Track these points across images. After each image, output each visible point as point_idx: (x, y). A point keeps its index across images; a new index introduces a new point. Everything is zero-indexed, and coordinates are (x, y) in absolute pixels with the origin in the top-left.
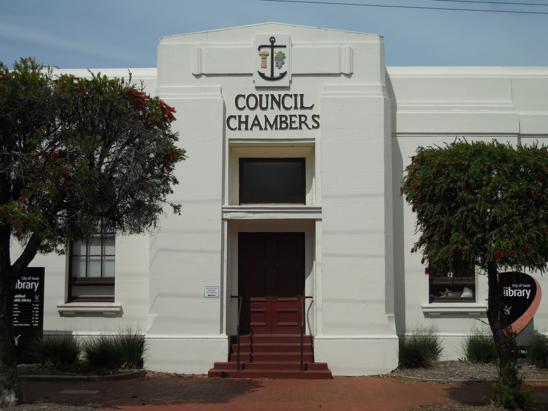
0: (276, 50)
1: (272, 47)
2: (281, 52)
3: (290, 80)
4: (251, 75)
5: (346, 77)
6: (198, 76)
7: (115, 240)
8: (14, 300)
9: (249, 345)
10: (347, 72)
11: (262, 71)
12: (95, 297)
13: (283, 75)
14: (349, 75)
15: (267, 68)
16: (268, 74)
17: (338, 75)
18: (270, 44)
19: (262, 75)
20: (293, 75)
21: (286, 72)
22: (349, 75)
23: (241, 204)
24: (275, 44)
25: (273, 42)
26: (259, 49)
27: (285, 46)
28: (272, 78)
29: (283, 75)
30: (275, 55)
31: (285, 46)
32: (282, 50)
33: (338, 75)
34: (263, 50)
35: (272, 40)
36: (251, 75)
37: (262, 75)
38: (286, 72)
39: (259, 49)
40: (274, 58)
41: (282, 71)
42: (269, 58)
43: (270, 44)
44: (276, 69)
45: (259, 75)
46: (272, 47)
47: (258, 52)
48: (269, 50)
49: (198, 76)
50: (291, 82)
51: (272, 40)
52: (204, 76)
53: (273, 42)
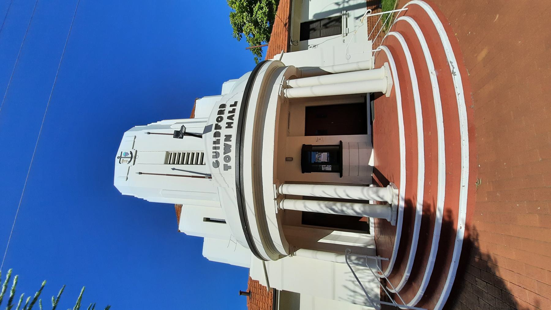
6: (127, 179)
10: (134, 138)
16: (129, 159)
17: (134, 141)
20: (133, 149)
26: (121, 163)
27: (122, 152)
30: (124, 157)
31: (122, 152)
32: (123, 153)
37: (130, 162)
39: (121, 163)
41: (129, 153)
42: (125, 159)
48: (122, 159)
49: (127, 179)
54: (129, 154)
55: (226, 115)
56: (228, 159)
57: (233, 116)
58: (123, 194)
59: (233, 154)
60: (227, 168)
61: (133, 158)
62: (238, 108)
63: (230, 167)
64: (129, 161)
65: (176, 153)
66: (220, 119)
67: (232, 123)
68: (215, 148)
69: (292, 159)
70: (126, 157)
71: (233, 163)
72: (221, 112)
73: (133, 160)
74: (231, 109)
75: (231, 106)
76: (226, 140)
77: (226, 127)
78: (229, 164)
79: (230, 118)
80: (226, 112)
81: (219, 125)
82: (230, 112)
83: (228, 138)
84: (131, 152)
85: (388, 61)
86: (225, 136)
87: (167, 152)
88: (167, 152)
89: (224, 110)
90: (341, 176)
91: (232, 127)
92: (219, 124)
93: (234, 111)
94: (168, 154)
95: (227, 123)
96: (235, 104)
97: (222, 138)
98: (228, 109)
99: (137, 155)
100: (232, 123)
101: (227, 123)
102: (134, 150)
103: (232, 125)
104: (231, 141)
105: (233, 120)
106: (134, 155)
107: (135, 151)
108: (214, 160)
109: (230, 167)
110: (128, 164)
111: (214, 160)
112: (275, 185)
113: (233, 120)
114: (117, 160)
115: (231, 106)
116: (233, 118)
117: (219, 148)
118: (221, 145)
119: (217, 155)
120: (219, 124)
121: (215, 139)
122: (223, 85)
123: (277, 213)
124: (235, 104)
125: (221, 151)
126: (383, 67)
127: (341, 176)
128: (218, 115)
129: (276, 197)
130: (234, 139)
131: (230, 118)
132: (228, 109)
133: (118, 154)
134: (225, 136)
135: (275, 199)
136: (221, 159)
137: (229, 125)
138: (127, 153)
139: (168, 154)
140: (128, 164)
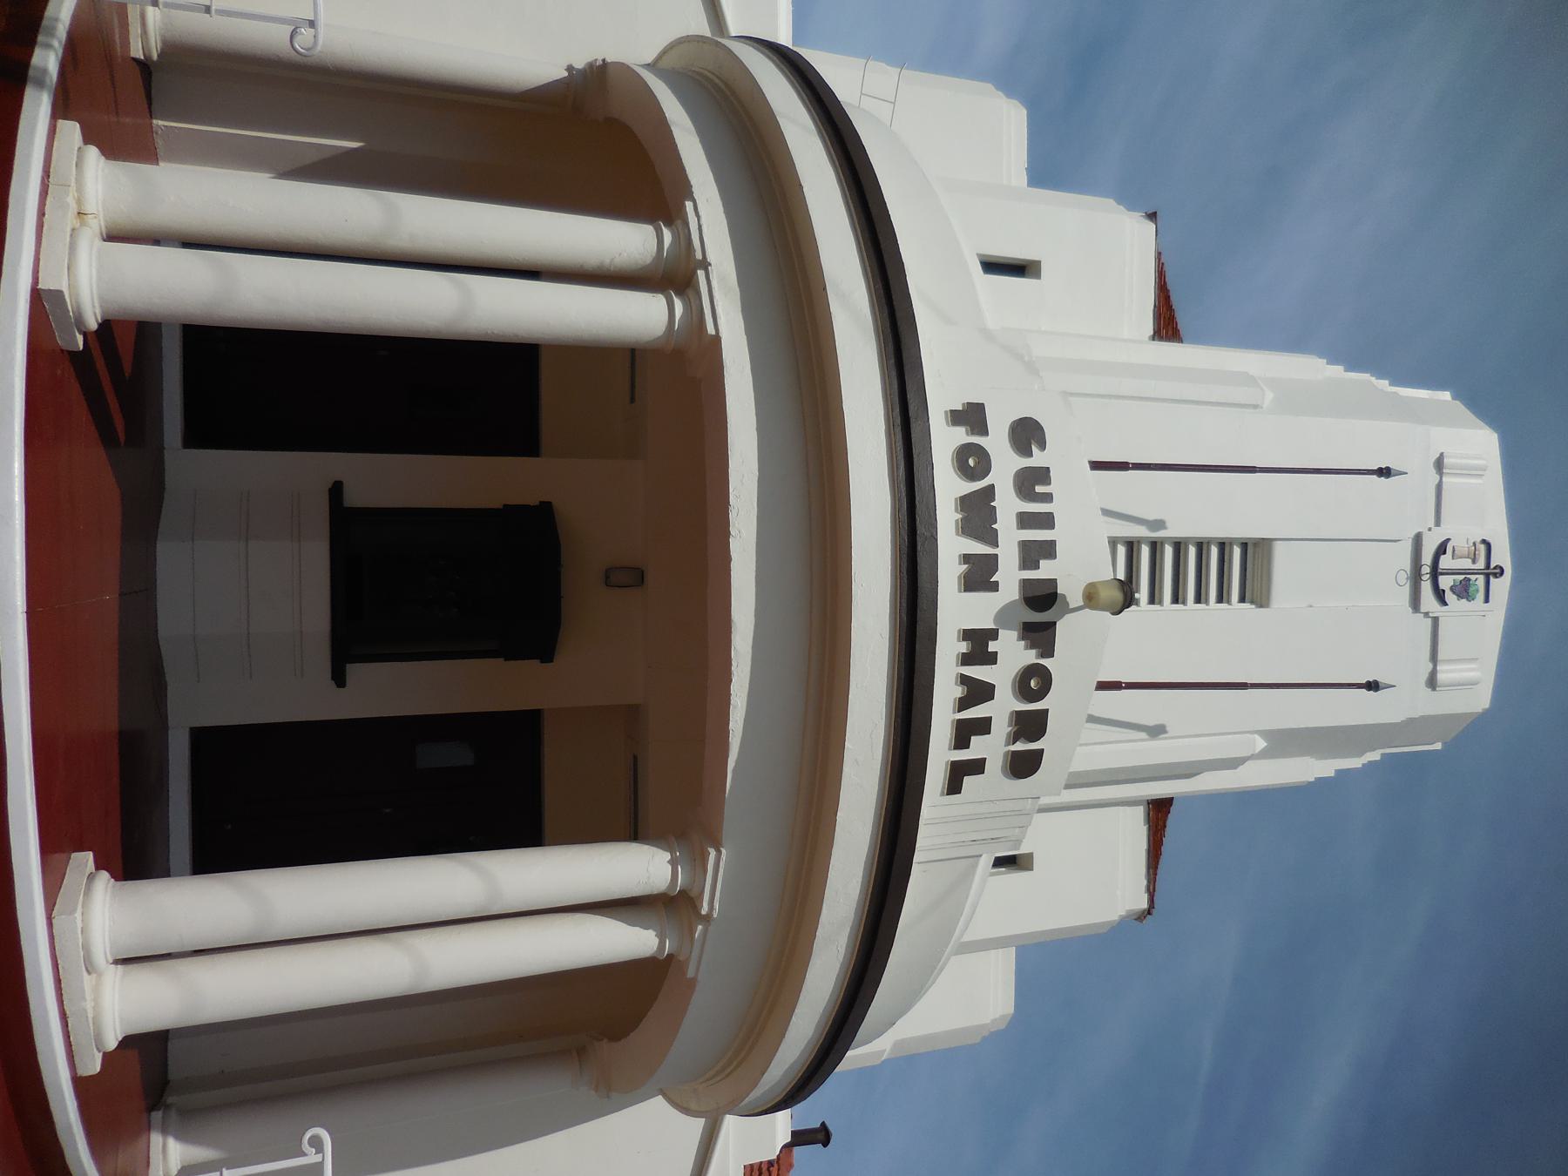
0: (1481, 578)
3: (1431, 615)
5: (1427, 675)
6: (1439, 464)
7: (1024, 854)
8: (700, 924)
9: (162, 164)
12: (277, 132)
13: (1440, 595)
14: (1432, 683)
15: (1453, 559)
16: (1446, 562)
20: (1436, 620)
21: (1447, 605)
22: (1432, 683)
23: (355, 671)
24: (1491, 578)
27: (1487, 600)
28: (1435, 573)
30: (1473, 577)
31: (1487, 600)
32: (1481, 595)
34: (1482, 548)
35: (1500, 572)
37: (1442, 549)
38: (1447, 605)
39: (1484, 541)
40: (1468, 576)
41: (1449, 596)
42: (1466, 564)
47: (1479, 540)
48: (1481, 564)
49: (1439, 464)
50: (1426, 614)
52: (1431, 666)
54: (1452, 589)
55: (1003, 707)
56: (972, 462)
57: (963, 704)
58: (1446, 396)
59: (948, 487)
60: (972, 417)
61: (1426, 570)
62: (940, 753)
63: (956, 418)
64: (1445, 553)
65: (1220, 599)
66: (1034, 682)
67: (966, 660)
68: (1043, 475)
69: (607, 577)
70: (1463, 577)
71: (944, 440)
72: (1031, 725)
73: (1427, 559)
74: (979, 747)
75: (977, 767)
76: (991, 563)
77: (993, 634)
78: (960, 436)
79: (978, 692)
80: (1002, 726)
81: (1032, 647)
82: (983, 726)
83: (979, 576)
84: (1444, 603)
85: (80, 1083)
86: (994, 587)
87: (1262, 601)
88: (1262, 601)
89: (1015, 737)
90: (336, 490)
91: (968, 635)
92: (1031, 657)
93: (964, 733)
94: (1255, 591)
95: (991, 659)
96: (958, 775)
97: (1010, 576)
98: (991, 748)
99: (1406, 590)
100: (966, 660)
101: (991, 659)
102: (1430, 529)
103: (964, 647)
104: (966, 558)
105: (964, 680)
106: (1426, 586)
107: (1423, 609)
108: (1038, 459)
109: (956, 418)
110: (1449, 540)
111: (1038, 459)
112: (711, 330)
113: (964, 680)
114: (1503, 556)
115: (977, 767)
116: (959, 692)
117: (1025, 520)
118: (1010, 537)
119: (1031, 482)
120: (1031, 657)
121: (1046, 570)
122: (1011, 1010)
123: (689, 205)
124: (958, 775)
125: (1008, 505)
126: (111, 1044)
127: (336, 490)
128: (1041, 752)
129: (701, 273)
130: (949, 571)
131: (978, 692)
132: (991, 748)
133: (1501, 587)
134: (994, 587)
135: (705, 264)
136: (1005, 464)
137: (979, 646)
138: (1460, 596)
139: (1255, 591)
140: (1449, 540)
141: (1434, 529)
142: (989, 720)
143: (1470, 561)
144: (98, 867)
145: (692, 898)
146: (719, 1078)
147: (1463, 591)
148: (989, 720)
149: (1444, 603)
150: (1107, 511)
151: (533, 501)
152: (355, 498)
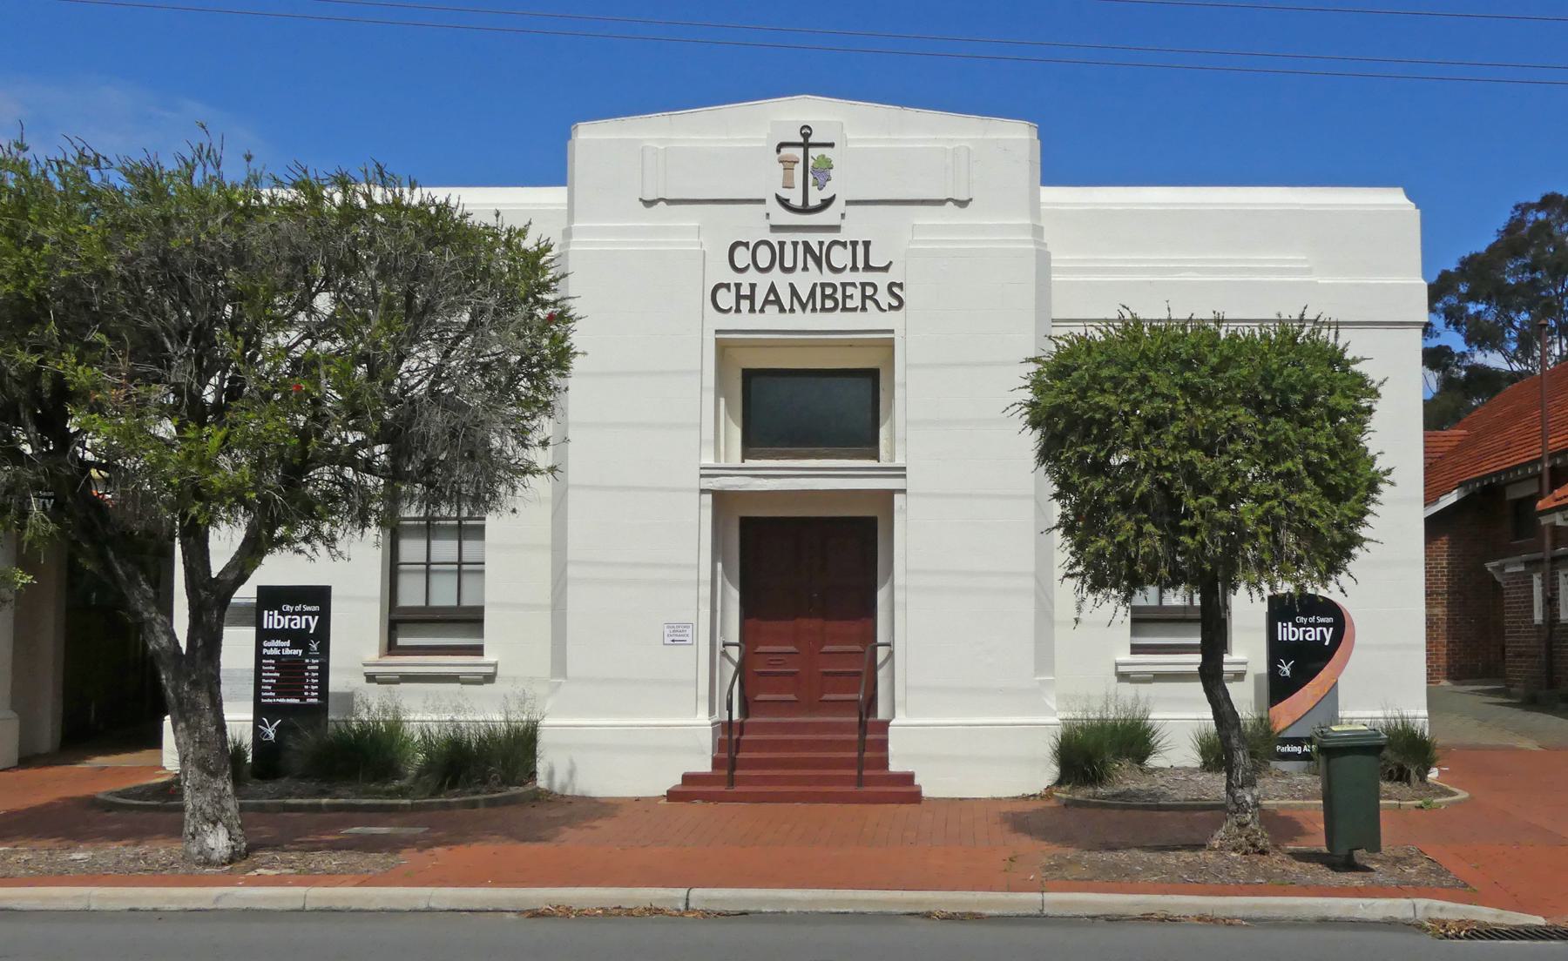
0: (813, 152)
1: (806, 145)
2: (824, 156)
4: (762, 201)
6: (649, 203)
11: (785, 194)
13: (826, 203)
14: (962, 204)
16: (797, 201)
17: (941, 202)
18: (801, 140)
19: (784, 203)
20: (848, 203)
24: (811, 140)
25: (806, 136)
26: (778, 151)
27: (831, 145)
28: (805, 209)
29: (826, 203)
30: (811, 162)
31: (831, 145)
33: (941, 202)
34: (785, 151)
35: (806, 131)
36: (762, 201)
37: (784, 203)
39: (778, 151)
41: (826, 194)
43: (801, 140)
44: (812, 190)
45: (775, 200)
46: (806, 145)
48: (798, 153)
49: (649, 203)
51: (806, 131)
53: (806, 136)
70: (810, 177)
84: (832, 199)
110: (776, 195)
141: (767, 224)
142: (779, 242)
143: (796, 165)
144: (1374, 458)
145: (1036, 577)
146: (1499, 700)
147: (822, 173)
148: (779, 242)
149: (832, 199)
150: (710, 713)
151: (348, 690)
152: (876, 461)
